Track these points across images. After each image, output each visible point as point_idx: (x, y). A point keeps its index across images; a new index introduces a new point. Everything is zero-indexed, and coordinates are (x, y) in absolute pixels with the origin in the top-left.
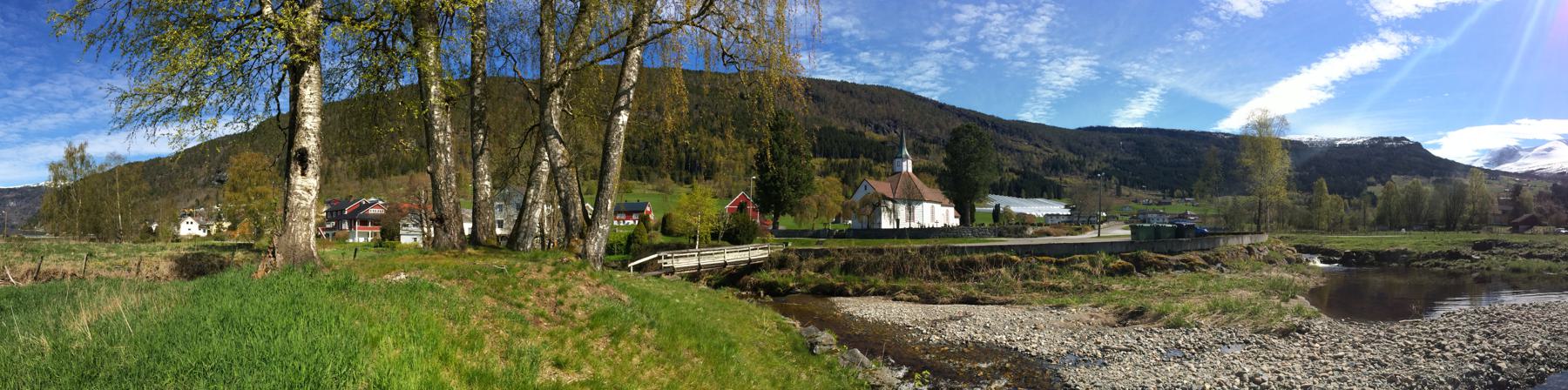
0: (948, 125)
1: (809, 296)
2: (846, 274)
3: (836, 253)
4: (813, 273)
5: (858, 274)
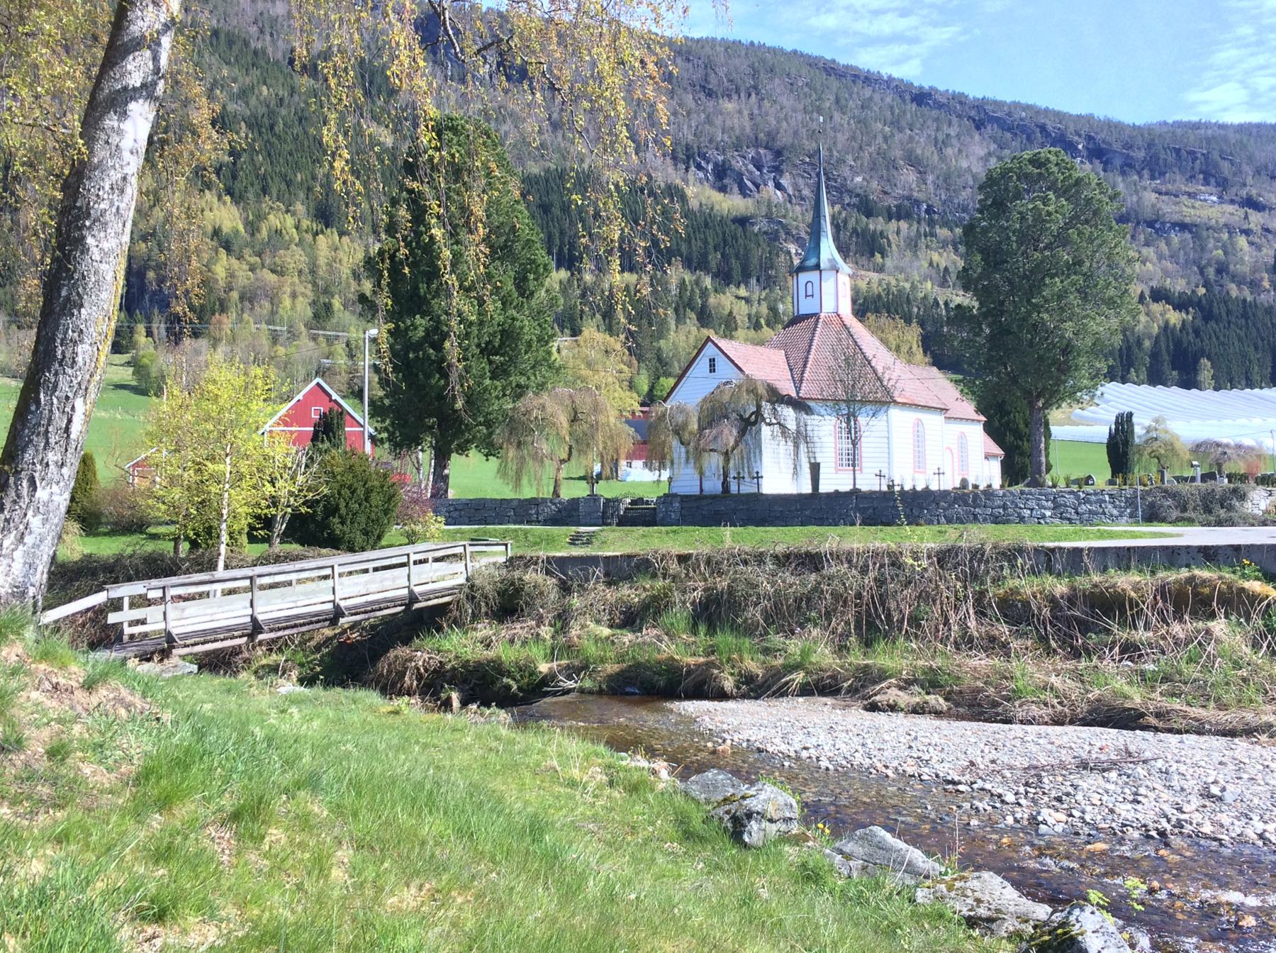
0: (943, 159)
1: (605, 699)
2: (711, 631)
3: (674, 567)
4: (606, 632)
5: (749, 630)
